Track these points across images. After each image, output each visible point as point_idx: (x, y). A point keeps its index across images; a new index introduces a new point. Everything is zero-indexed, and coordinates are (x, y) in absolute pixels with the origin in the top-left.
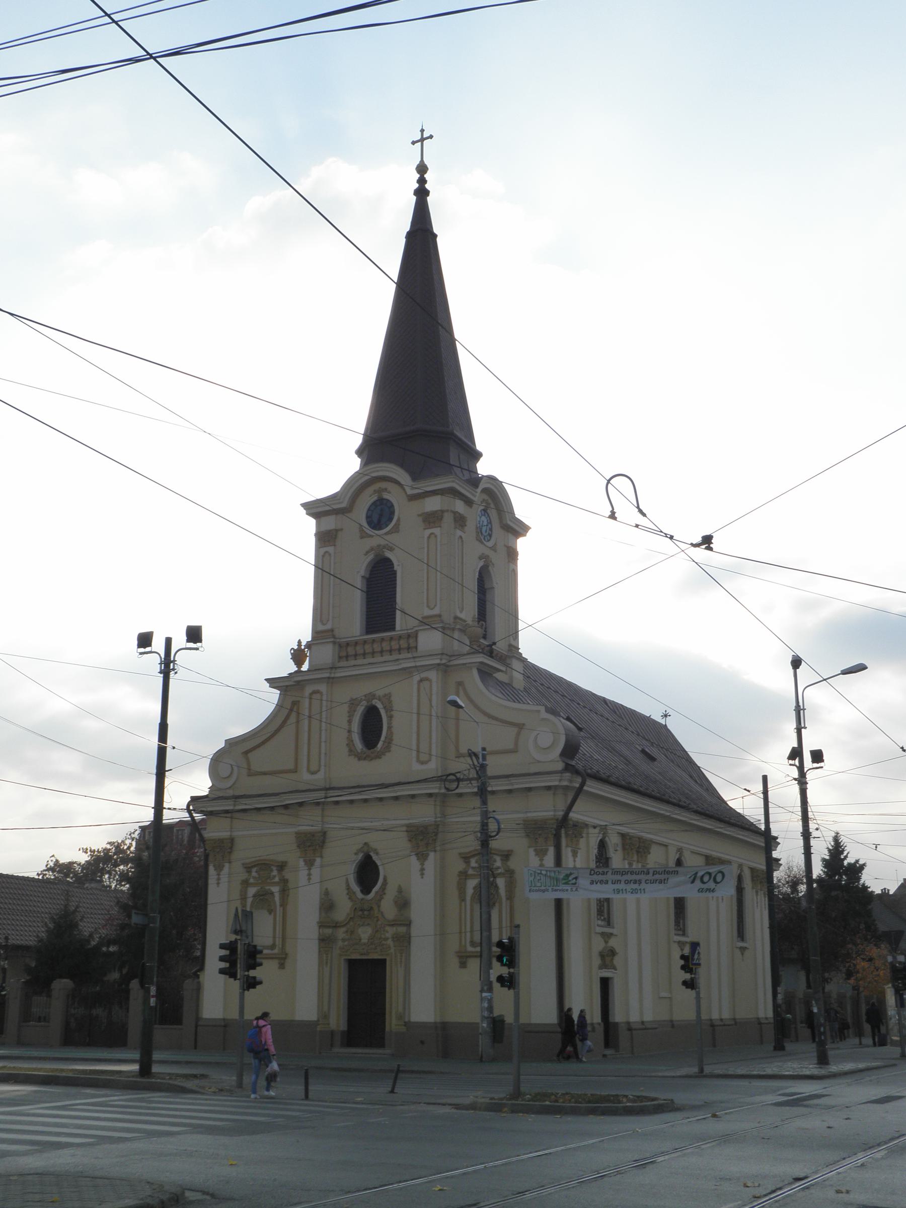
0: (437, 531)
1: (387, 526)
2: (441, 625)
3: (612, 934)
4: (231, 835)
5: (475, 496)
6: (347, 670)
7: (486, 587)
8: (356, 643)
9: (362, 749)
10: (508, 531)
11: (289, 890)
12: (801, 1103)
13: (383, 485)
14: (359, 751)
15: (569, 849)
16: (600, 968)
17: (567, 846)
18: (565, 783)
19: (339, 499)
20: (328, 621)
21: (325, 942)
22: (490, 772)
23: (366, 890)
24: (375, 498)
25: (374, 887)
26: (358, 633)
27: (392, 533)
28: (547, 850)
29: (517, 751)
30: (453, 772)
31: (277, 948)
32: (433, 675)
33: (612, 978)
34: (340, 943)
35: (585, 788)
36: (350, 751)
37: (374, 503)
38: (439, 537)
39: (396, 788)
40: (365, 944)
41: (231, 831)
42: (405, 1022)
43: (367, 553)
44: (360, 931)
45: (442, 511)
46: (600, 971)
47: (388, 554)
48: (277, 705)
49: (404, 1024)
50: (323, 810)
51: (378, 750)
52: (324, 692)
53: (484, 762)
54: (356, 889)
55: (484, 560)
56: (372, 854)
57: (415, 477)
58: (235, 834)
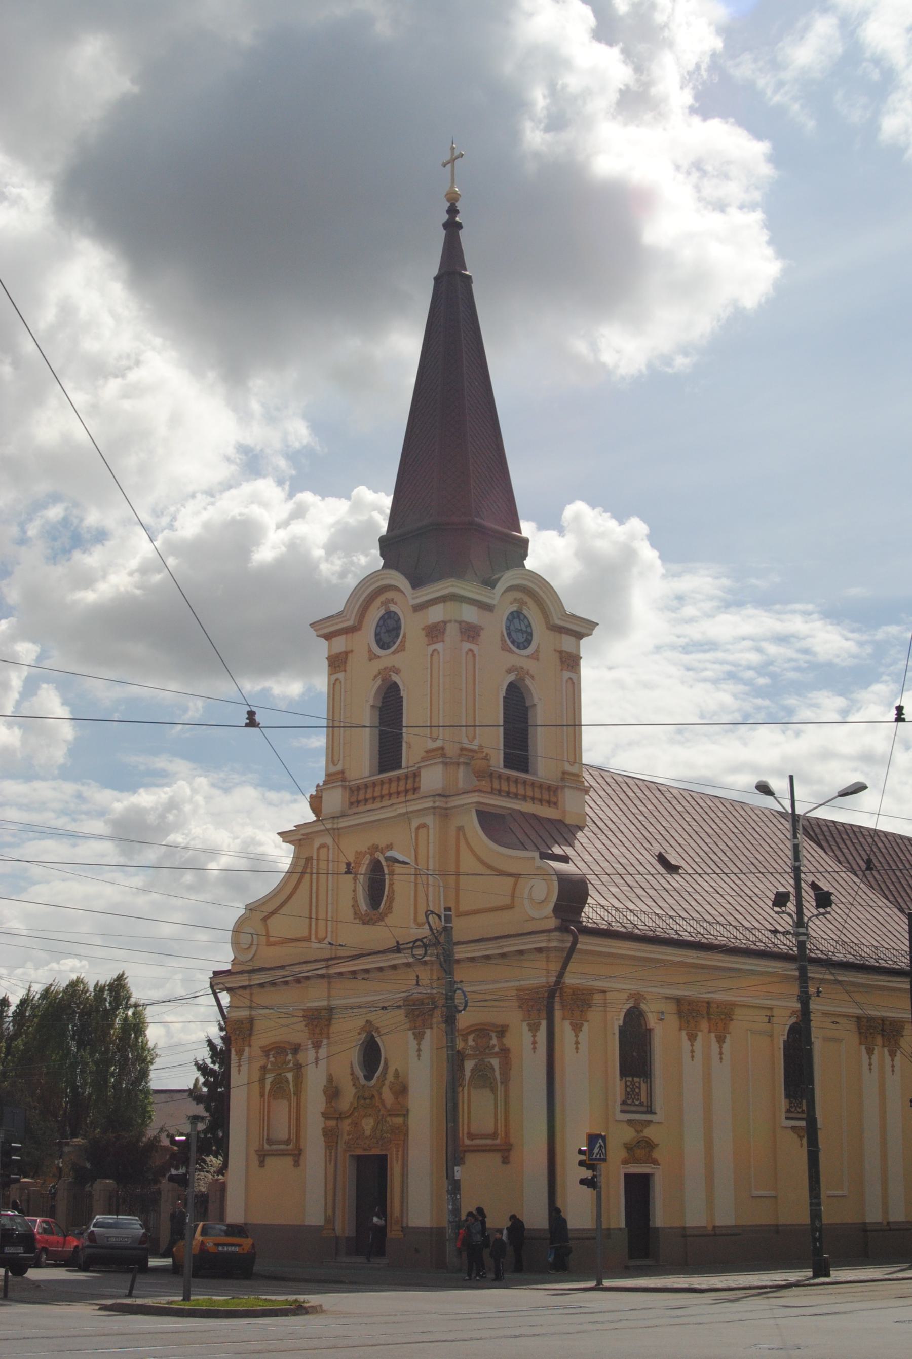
0: (439, 646)
1: (395, 643)
2: (440, 760)
3: (651, 1121)
4: (250, 1015)
5: (493, 598)
6: (364, 815)
7: (527, 704)
8: (366, 786)
9: (366, 910)
10: (561, 633)
11: (259, 1080)
12: (101, 1306)
13: (382, 598)
14: (363, 913)
15: (567, 1024)
16: (625, 1162)
17: (564, 1019)
18: (554, 944)
19: (345, 616)
20: (339, 760)
21: (330, 1136)
22: (456, 937)
23: (368, 1077)
24: (382, 612)
25: (376, 1072)
26: (367, 773)
27: (398, 652)
28: (540, 1024)
29: (513, 908)
30: (420, 938)
31: (499, 1137)
32: (429, 820)
33: (653, 1174)
34: (346, 1137)
35: (579, 946)
36: (355, 913)
37: (382, 618)
38: (441, 654)
39: (503, 942)
40: (367, 1138)
41: (329, 1000)
42: (402, 1227)
43: (375, 677)
44: (364, 1122)
45: (445, 623)
46: (622, 1166)
47: (395, 678)
48: (291, 865)
49: (401, 1229)
50: (329, 983)
51: (381, 911)
52: (331, 847)
53: (448, 925)
54: (360, 1074)
55: (516, 673)
56: (375, 1034)
57: (416, 583)
58: (254, 1013)
